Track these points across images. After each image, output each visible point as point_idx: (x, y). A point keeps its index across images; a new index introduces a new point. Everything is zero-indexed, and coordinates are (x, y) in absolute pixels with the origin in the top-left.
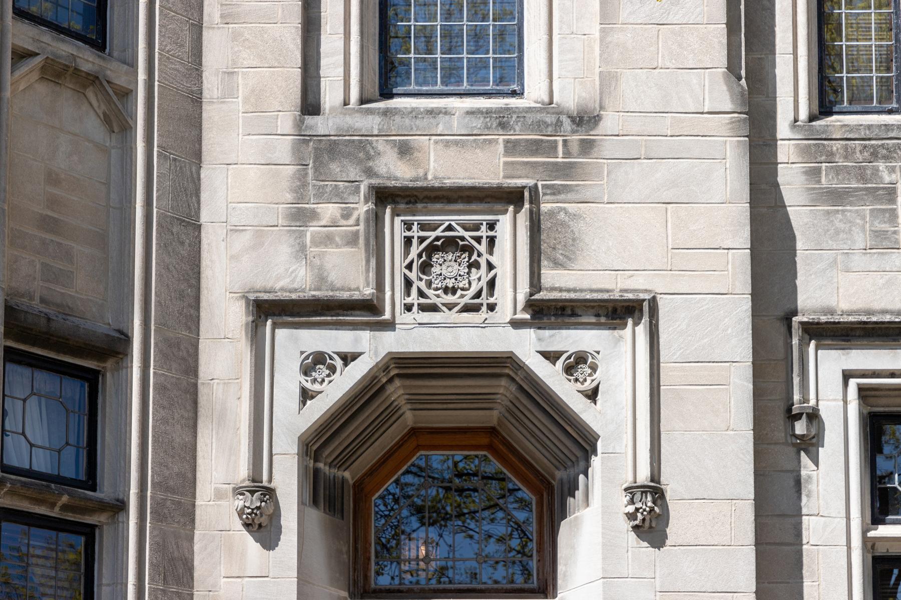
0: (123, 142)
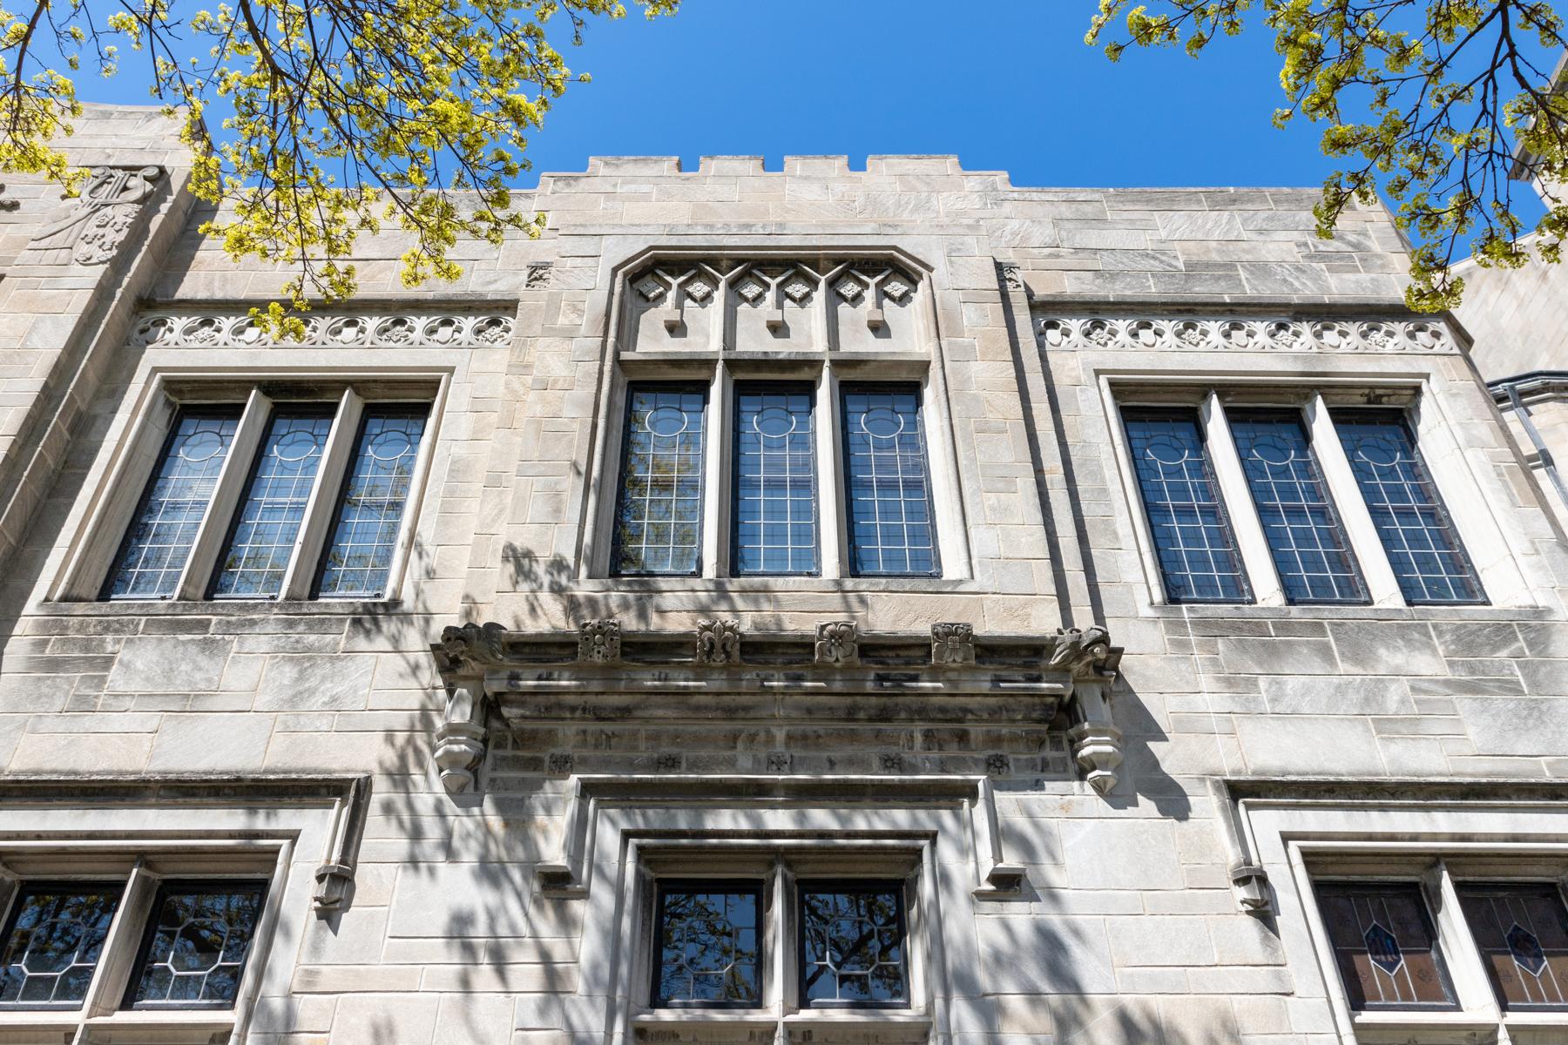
0: (45, 505)
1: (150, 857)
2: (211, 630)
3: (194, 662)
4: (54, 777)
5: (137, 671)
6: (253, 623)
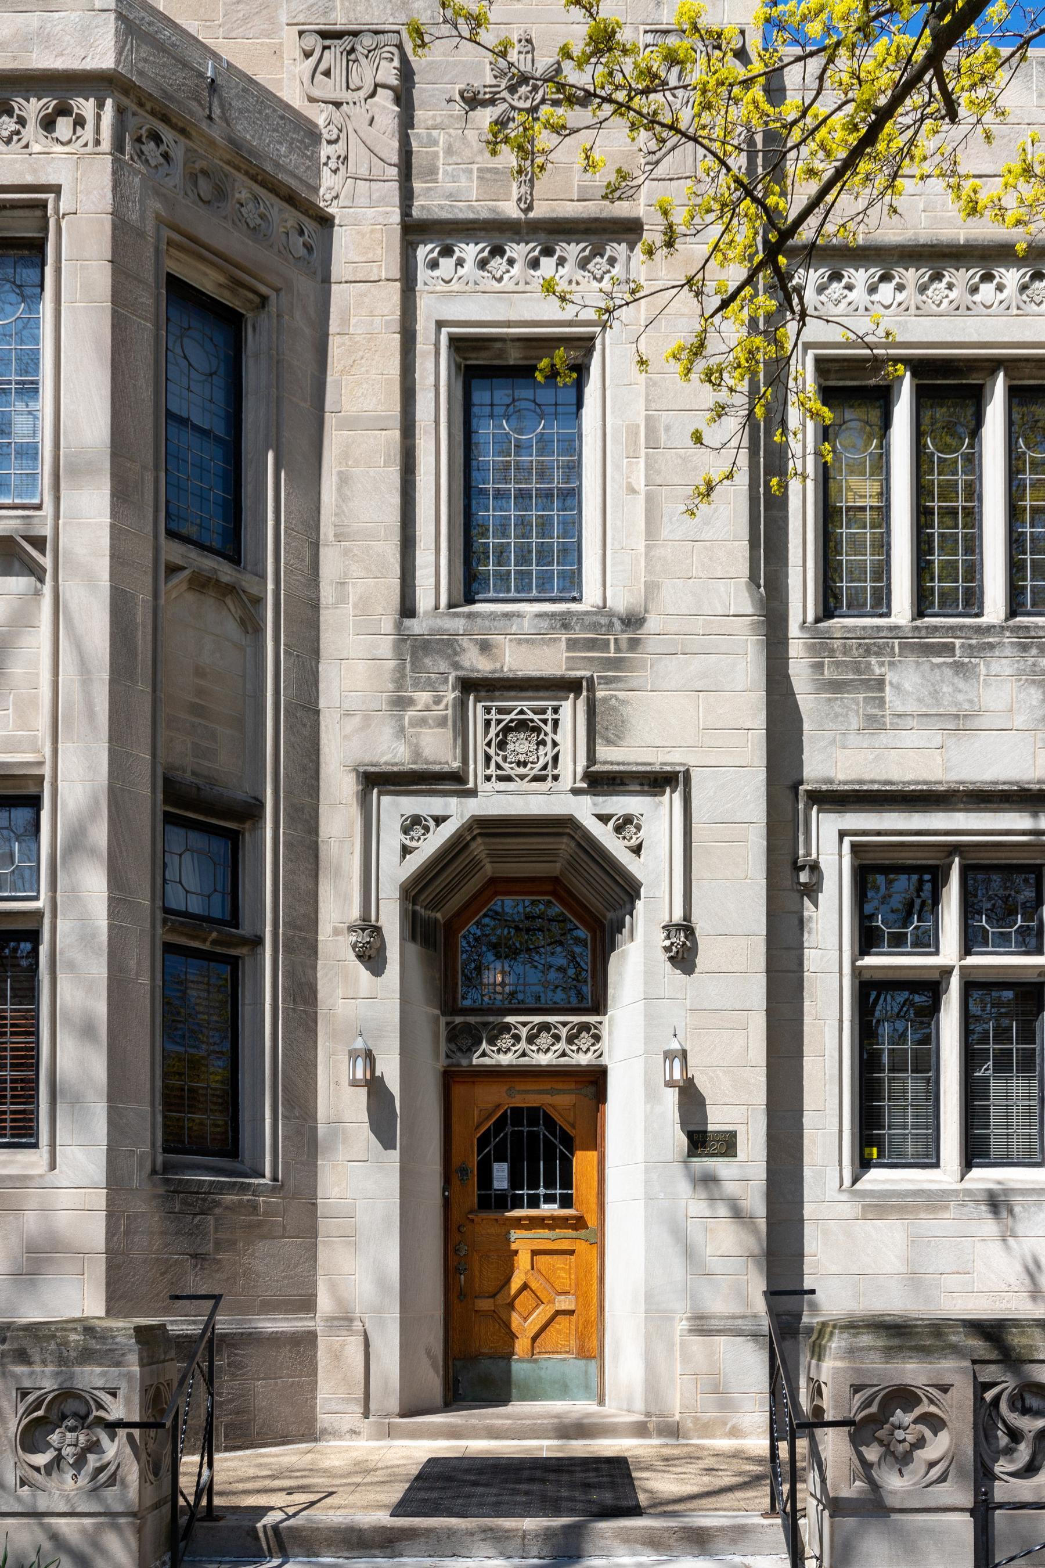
1: (962, 849)
2: (958, 652)
3: (953, 684)
4: (876, 787)
5: (908, 693)
6: (991, 646)
